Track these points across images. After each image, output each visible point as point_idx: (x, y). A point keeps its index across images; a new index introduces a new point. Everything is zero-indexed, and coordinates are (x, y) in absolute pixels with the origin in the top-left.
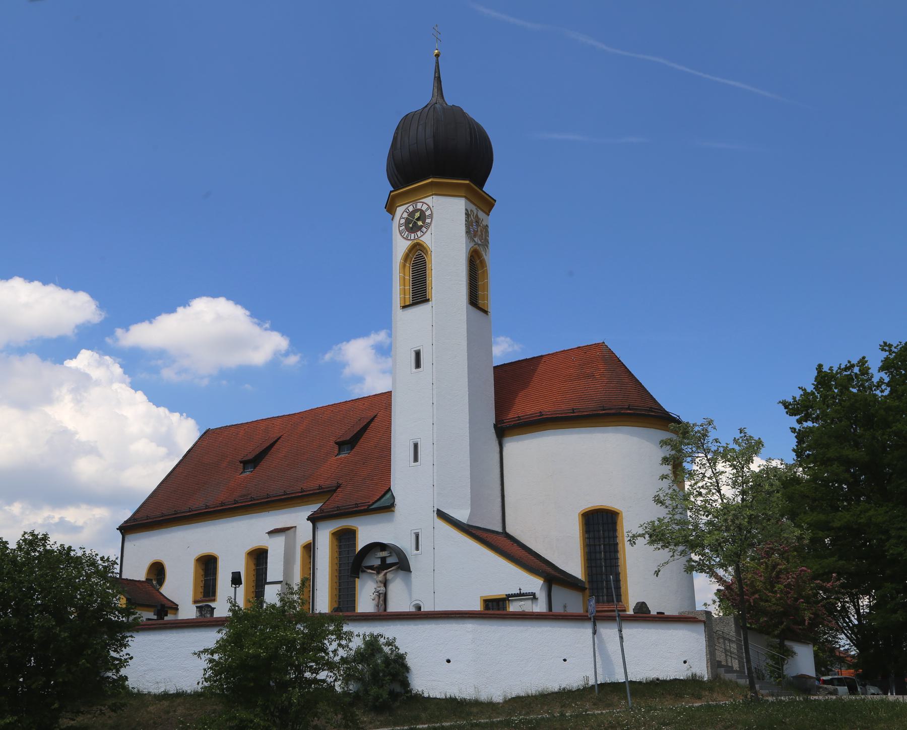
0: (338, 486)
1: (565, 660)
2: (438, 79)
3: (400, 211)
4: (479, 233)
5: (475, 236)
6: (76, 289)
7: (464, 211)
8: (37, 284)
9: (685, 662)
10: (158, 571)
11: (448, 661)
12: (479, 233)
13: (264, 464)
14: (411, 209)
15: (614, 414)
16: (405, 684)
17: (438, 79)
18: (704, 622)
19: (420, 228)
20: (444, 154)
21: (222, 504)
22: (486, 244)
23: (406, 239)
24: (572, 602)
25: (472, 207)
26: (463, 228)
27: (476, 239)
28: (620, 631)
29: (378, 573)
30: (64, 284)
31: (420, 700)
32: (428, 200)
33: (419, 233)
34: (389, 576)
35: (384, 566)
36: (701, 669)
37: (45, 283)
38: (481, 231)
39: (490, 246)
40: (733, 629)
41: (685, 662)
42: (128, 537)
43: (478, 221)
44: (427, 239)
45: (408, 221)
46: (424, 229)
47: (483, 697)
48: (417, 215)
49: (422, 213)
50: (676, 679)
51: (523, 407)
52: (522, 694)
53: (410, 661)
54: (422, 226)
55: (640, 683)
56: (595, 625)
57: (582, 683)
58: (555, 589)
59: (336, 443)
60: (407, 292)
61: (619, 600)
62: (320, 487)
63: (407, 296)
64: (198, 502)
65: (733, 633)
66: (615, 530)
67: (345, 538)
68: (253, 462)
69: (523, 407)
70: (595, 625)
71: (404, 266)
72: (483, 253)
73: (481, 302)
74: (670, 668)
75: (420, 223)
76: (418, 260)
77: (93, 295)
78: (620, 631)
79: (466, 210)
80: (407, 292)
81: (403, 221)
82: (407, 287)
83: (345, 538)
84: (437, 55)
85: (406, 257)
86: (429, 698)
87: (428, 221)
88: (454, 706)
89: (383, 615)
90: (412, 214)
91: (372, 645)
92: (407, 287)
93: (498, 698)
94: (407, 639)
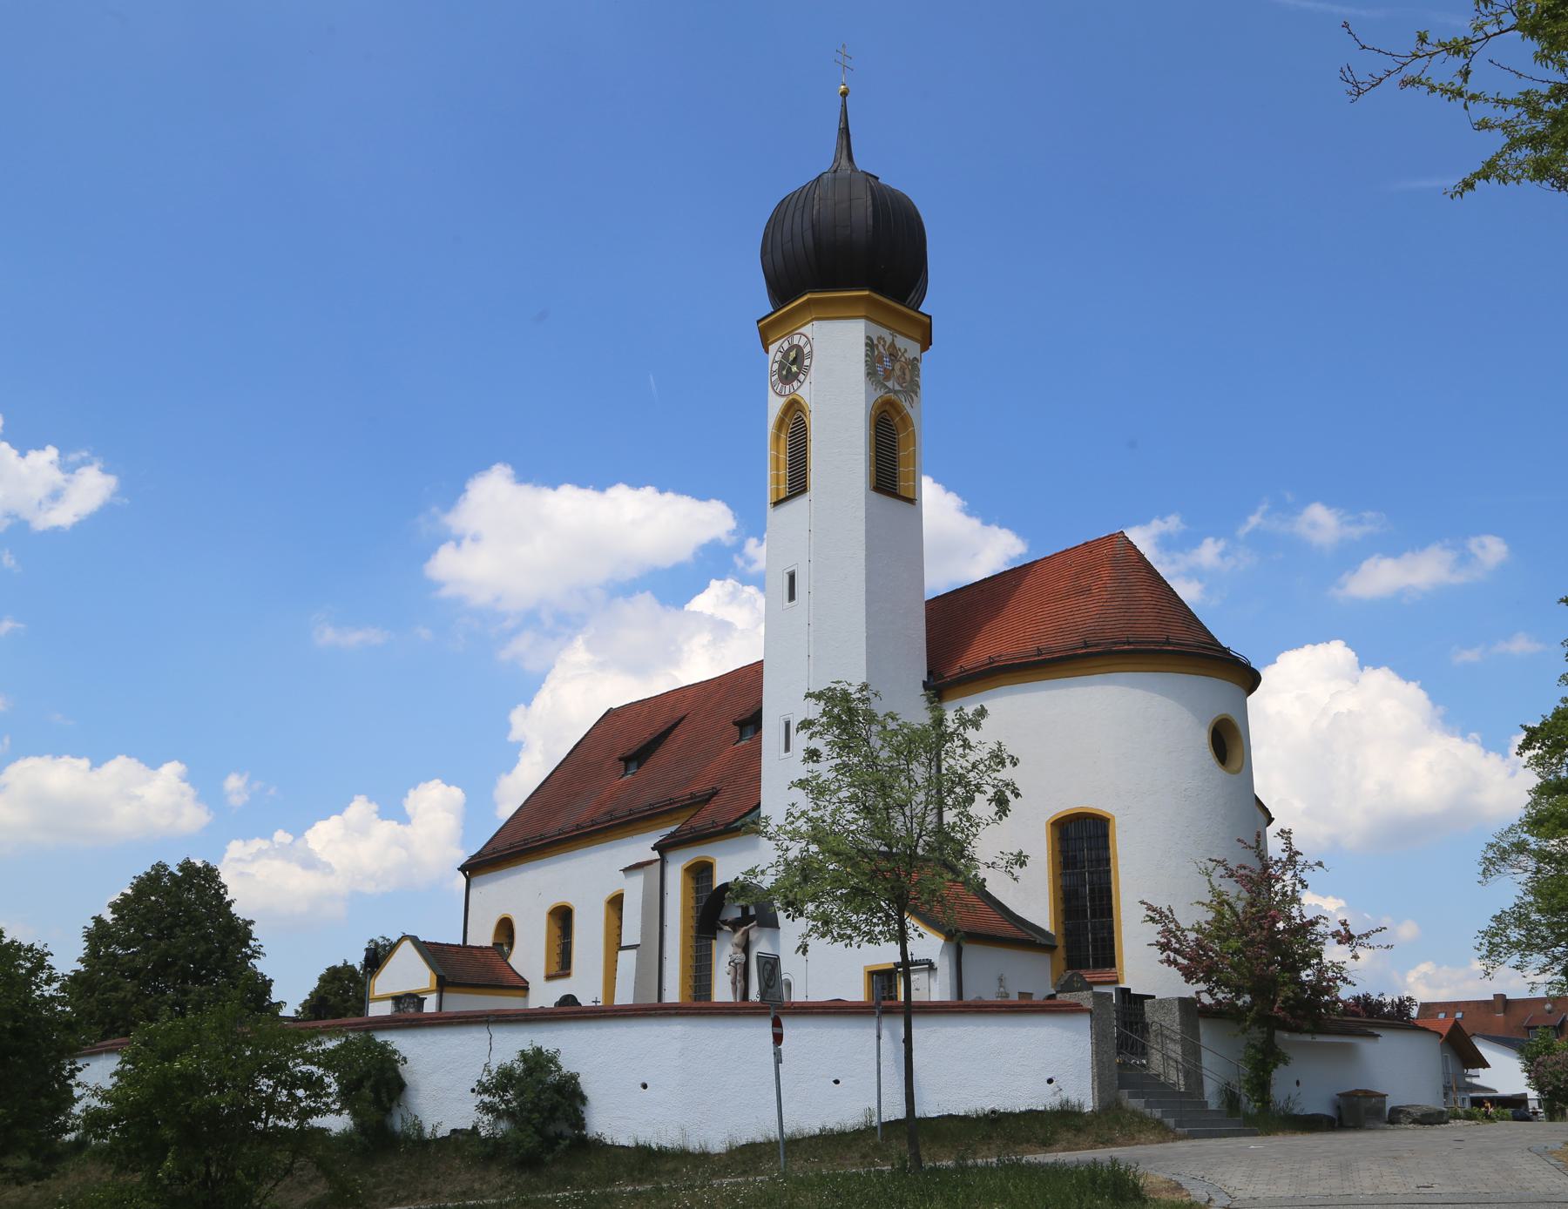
0: (715, 793)
1: (837, 1082)
2: (845, 132)
3: (773, 348)
4: (897, 372)
5: (887, 378)
6: (702, 495)
7: (863, 341)
8: (649, 492)
9: (1050, 1081)
10: (506, 928)
11: (645, 1086)
12: (897, 372)
13: (652, 761)
14: (786, 346)
15: (1183, 653)
16: (579, 1122)
17: (845, 132)
18: (1090, 1012)
19: (796, 376)
20: (854, 254)
21: (578, 827)
22: (912, 388)
23: (780, 395)
24: (1034, 975)
25: (879, 332)
26: (861, 369)
27: (889, 384)
28: (778, 1039)
29: (735, 931)
30: (680, 490)
31: (599, 1147)
32: (806, 330)
33: (795, 384)
34: (753, 935)
35: (745, 919)
36: (1081, 1092)
37: (662, 490)
38: (903, 370)
39: (922, 392)
40: (1178, 1020)
41: (1050, 1081)
42: (474, 880)
43: (894, 354)
44: (805, 391)
45: (782, 366)
46: (801, 377)
47: (693, 1145)
48: (793, 354)
49: (799, 349)
50: (1031, 1111)
51: (978, 653)
52: (760, 1139)
53: (588, 1086)
54: (797, 374)
55: (965, 1118)
56: (777, 1024)
57: (862, 1119)
58: (972, 953)
59: (735, 723)
60: (782, 479)
61: (1113, 965)
62: (693, 796)
63: (782, 487)
64: (553, 828)
65: (1177, 1027)
66: (1107, 848)
67: (701, 872)
68: (638, 757)
69: (978, 653)
70: (777, 1024)
71: (778, 438)
72: (907, 405)
73: (903, 486)
74: (1022, 1093)
75: (794, 369)
76: (795, 423)
77: (731, 506)
78: (778, 1039)
79: (868, 337)
80: (782, 479)
81: (776, 366)
82: (782, 472)
83: (701, 872)
84: (844, 94)
85: (781, 423)
86: (613, 1146)
87: (807, 362)
88: (646, 1159)
89: (568, 1011)
90: (786, 354)
91: (537, 1062)
92: (782, 472)
93: (717, 1145)
94: (574, 1049)
